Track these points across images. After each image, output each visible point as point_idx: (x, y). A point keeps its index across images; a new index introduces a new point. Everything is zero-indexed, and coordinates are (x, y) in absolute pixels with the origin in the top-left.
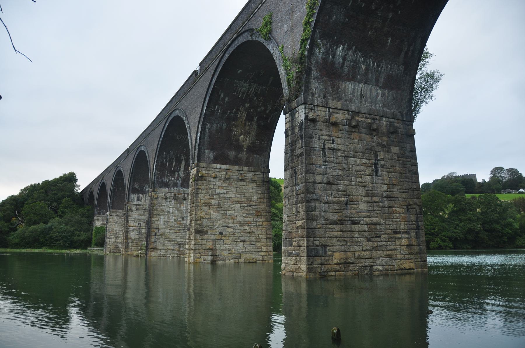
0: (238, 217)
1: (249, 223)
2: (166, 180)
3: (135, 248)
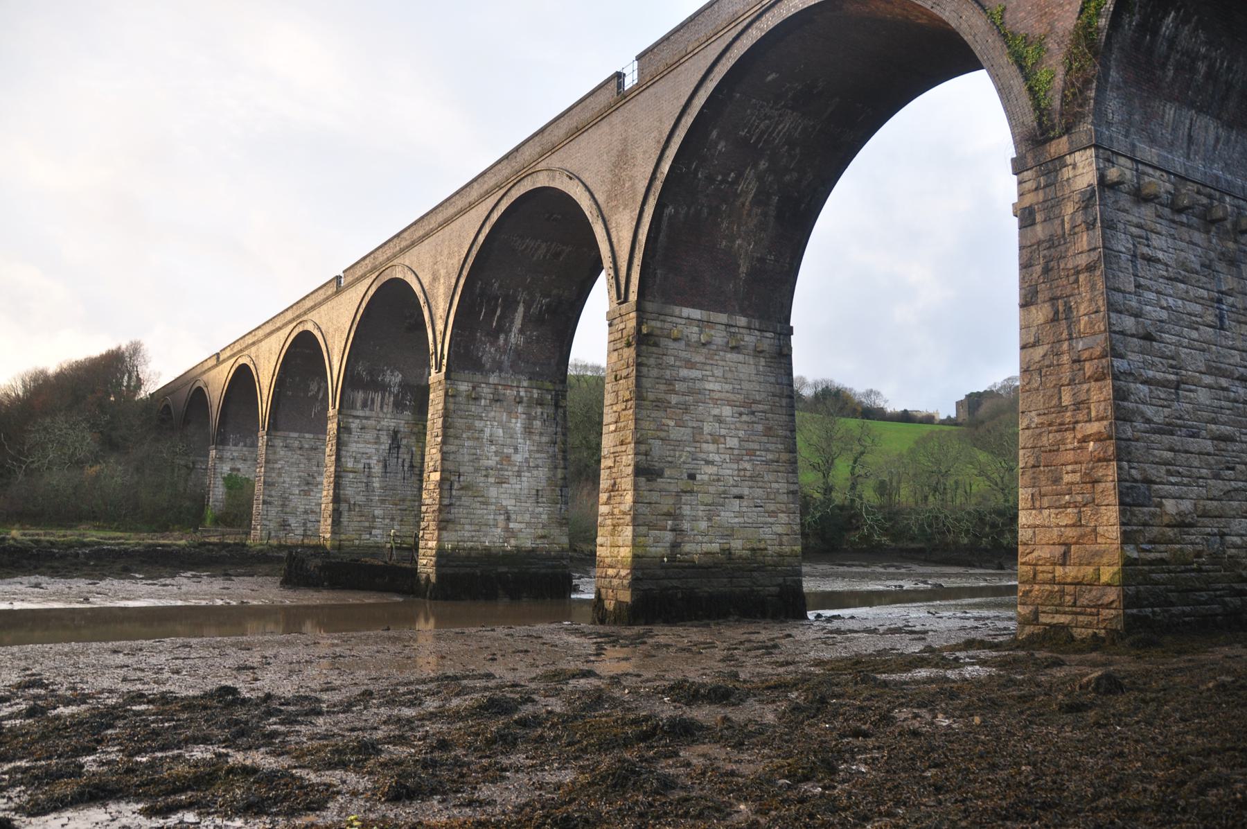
0: (728, 438)
1: (751, 453)
3: (356, 524)
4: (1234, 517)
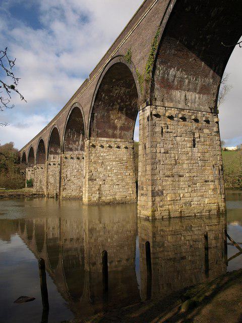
2: (70, 146)
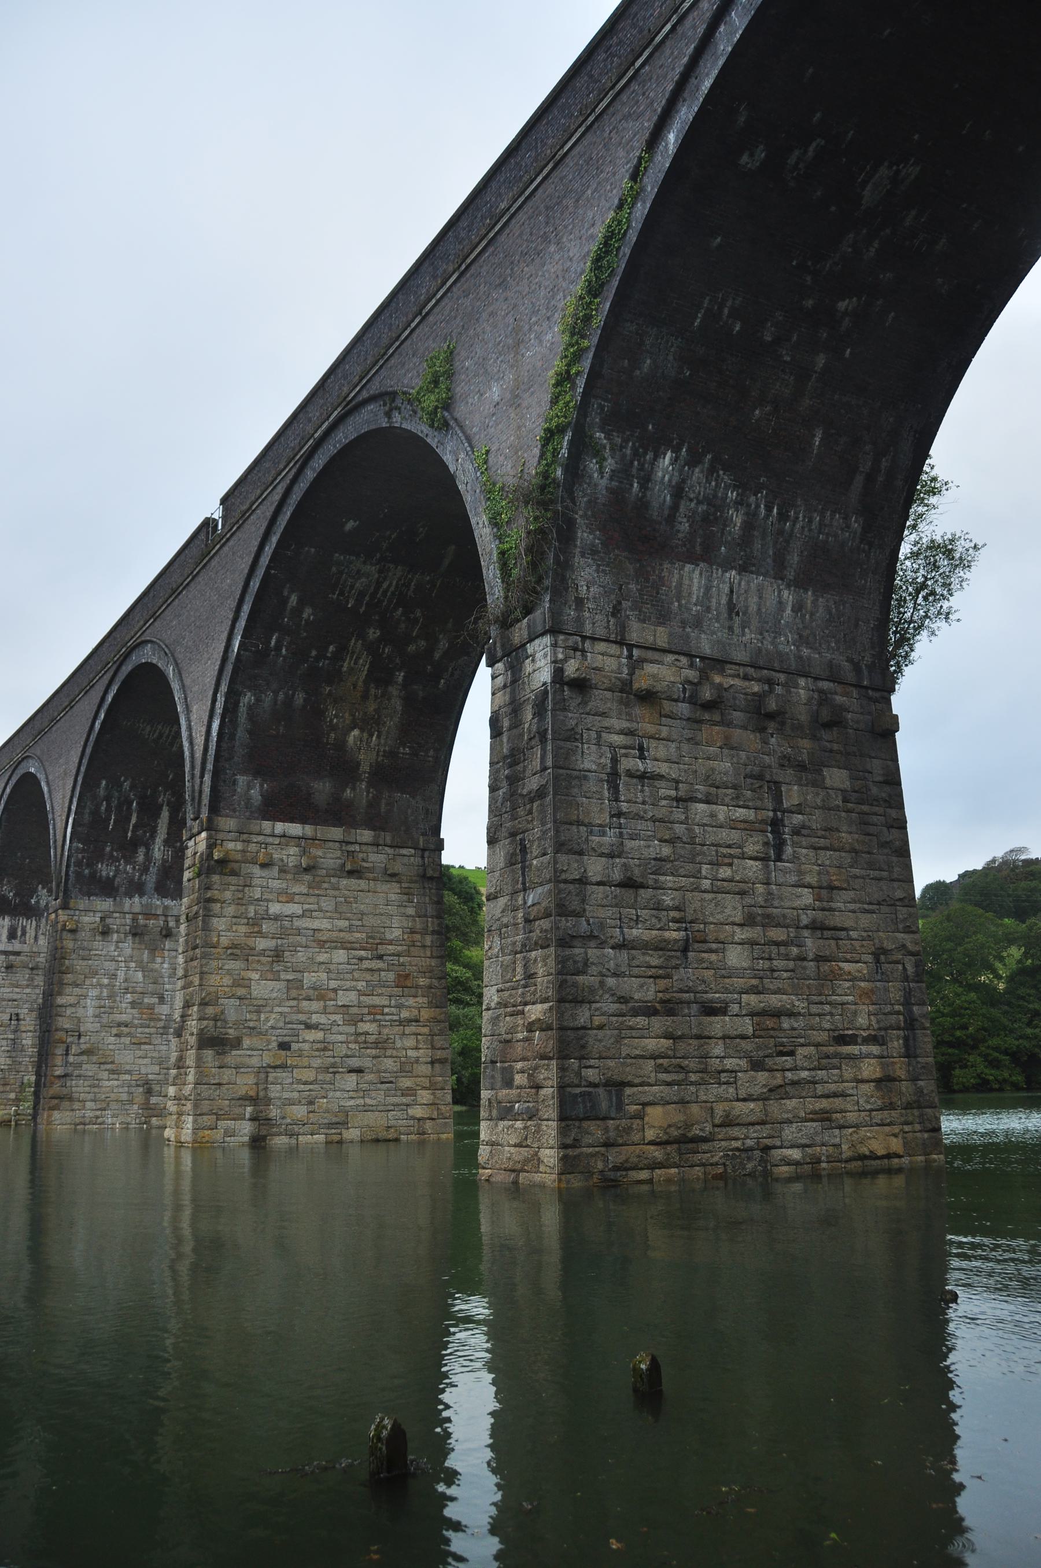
1: (375, 1011)
2: (105, 870)
4: (789, 1122)
